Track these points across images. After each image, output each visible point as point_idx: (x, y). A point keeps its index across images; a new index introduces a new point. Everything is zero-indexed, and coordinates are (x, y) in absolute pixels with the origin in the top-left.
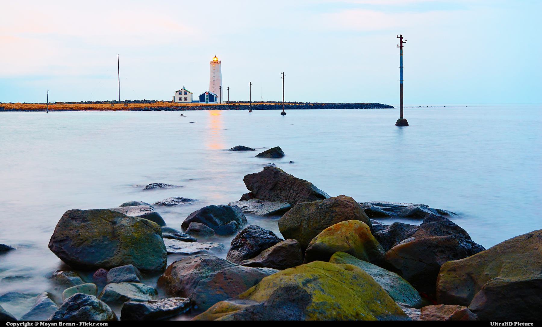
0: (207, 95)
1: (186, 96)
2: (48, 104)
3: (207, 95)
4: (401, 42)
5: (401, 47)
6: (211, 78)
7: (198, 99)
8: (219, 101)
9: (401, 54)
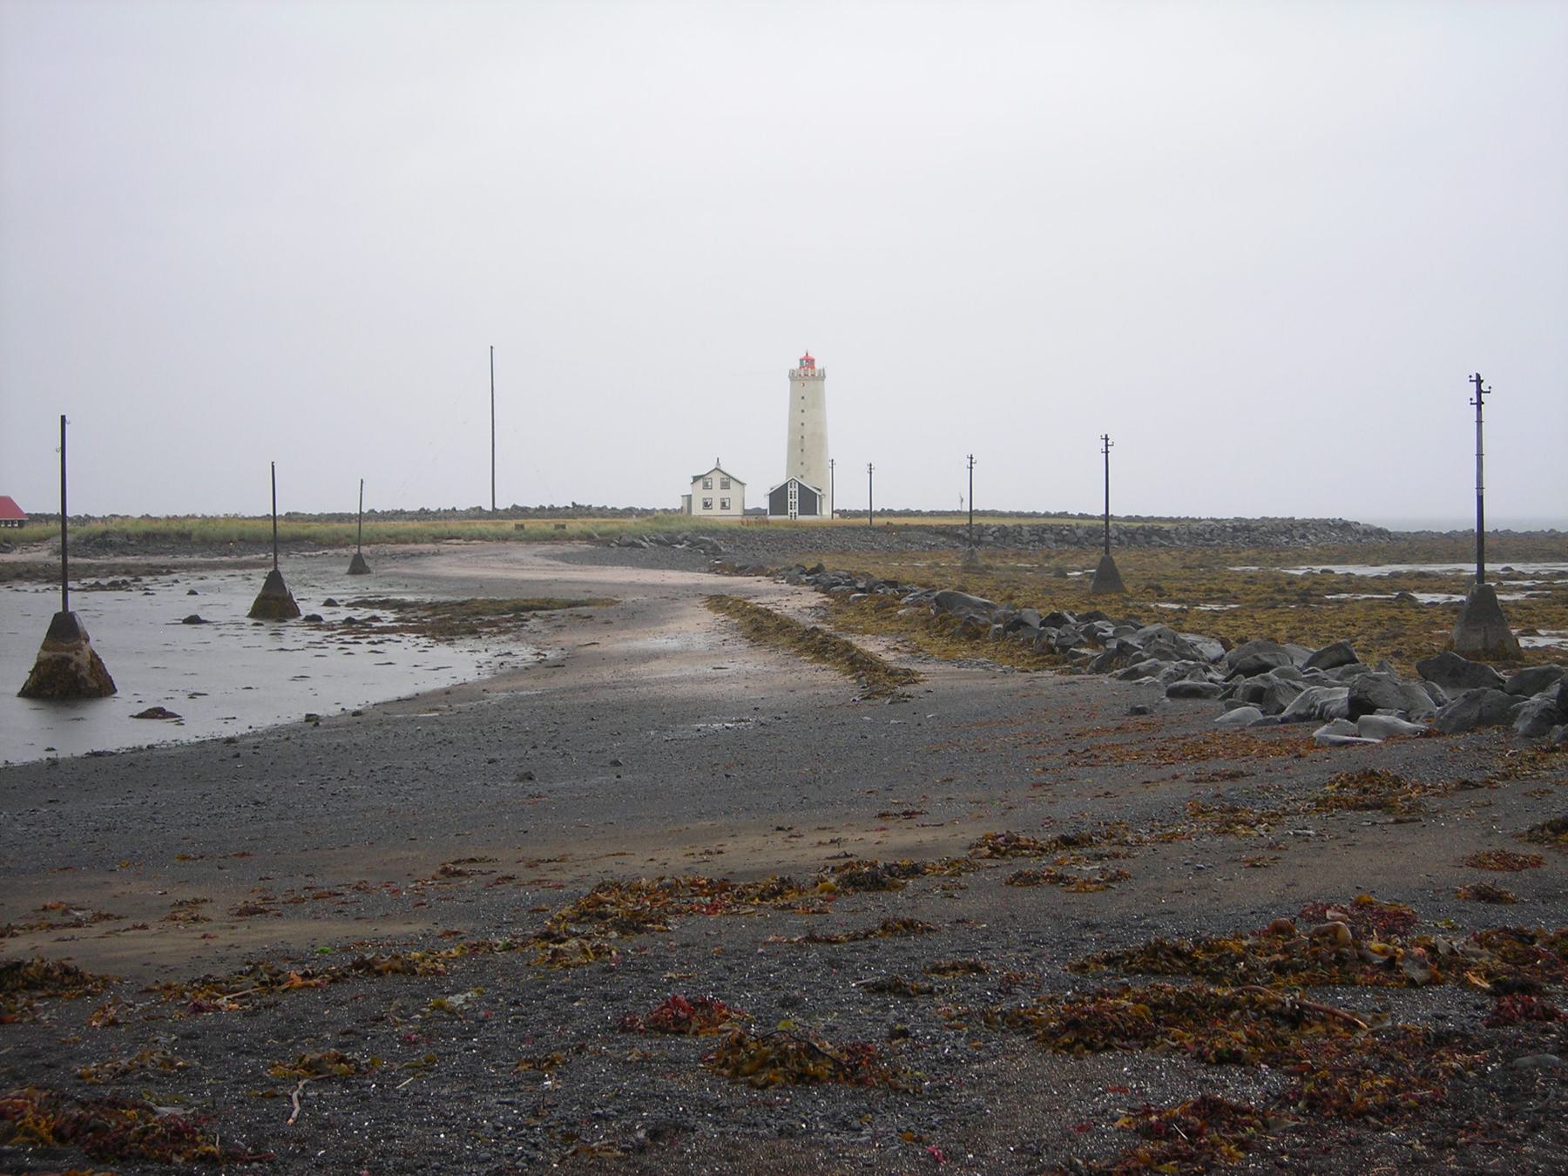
0: (793, 490)
1: (725, 494)
2: (361, 517)
3: (793, 490)
4: (1479, 392)
5: (1480, 404)
6: (791, 431)
7: (765, 505)
8: (826, 512)
9: (1479, 422)
